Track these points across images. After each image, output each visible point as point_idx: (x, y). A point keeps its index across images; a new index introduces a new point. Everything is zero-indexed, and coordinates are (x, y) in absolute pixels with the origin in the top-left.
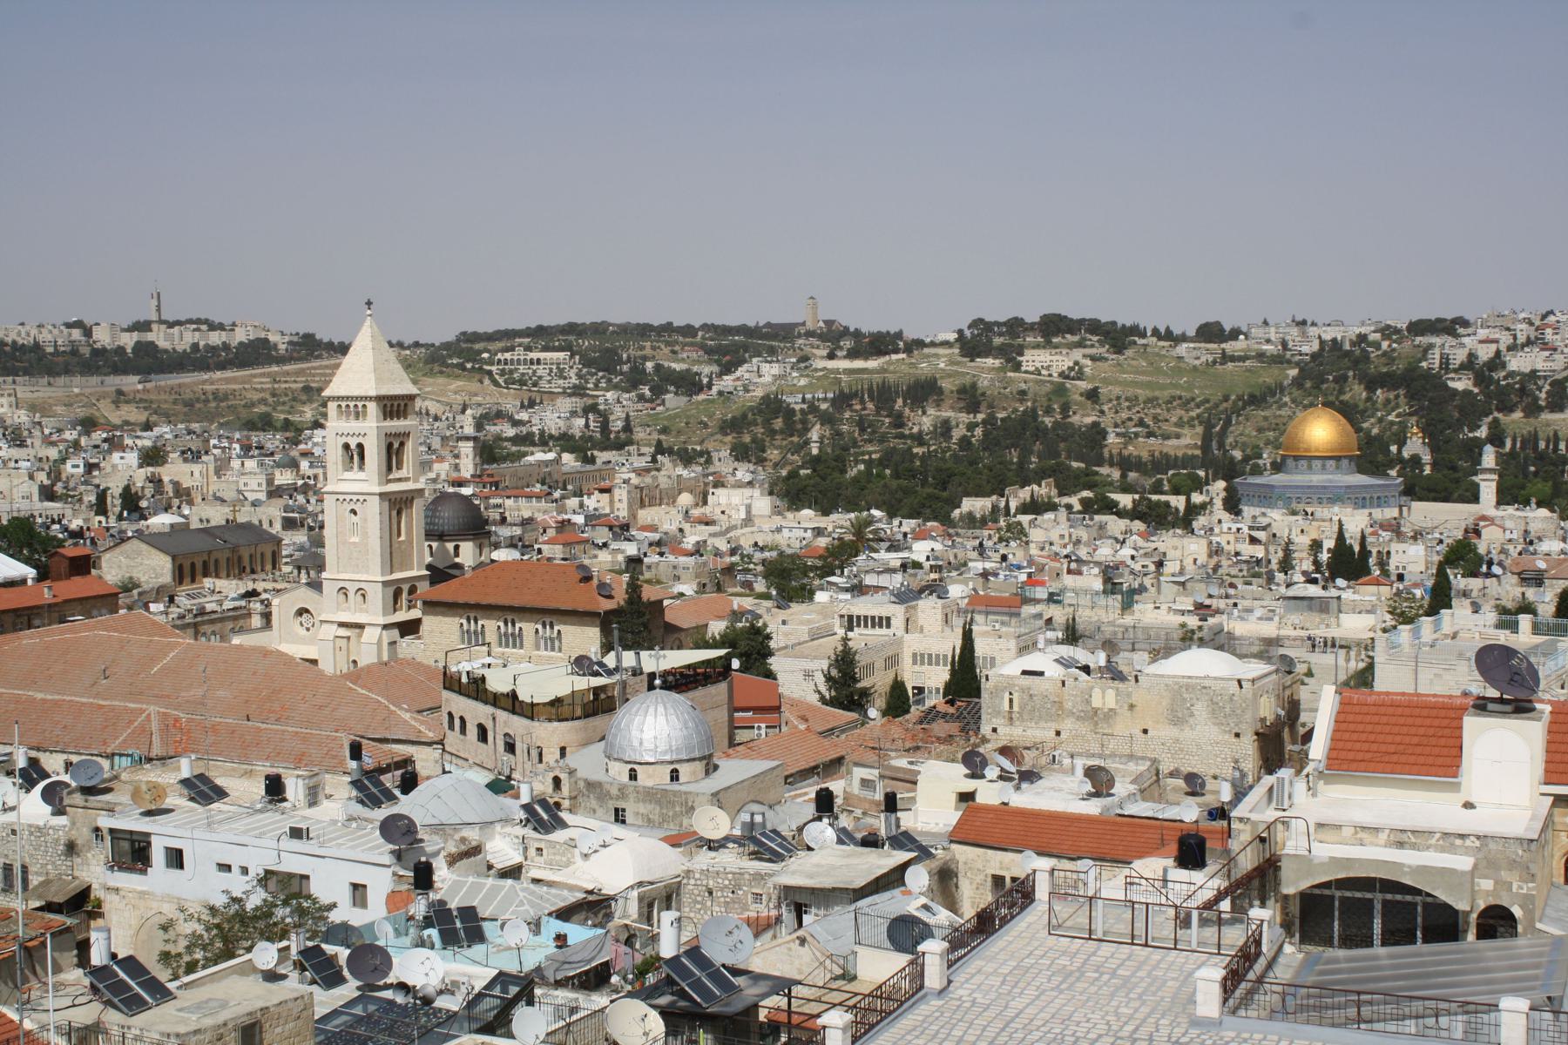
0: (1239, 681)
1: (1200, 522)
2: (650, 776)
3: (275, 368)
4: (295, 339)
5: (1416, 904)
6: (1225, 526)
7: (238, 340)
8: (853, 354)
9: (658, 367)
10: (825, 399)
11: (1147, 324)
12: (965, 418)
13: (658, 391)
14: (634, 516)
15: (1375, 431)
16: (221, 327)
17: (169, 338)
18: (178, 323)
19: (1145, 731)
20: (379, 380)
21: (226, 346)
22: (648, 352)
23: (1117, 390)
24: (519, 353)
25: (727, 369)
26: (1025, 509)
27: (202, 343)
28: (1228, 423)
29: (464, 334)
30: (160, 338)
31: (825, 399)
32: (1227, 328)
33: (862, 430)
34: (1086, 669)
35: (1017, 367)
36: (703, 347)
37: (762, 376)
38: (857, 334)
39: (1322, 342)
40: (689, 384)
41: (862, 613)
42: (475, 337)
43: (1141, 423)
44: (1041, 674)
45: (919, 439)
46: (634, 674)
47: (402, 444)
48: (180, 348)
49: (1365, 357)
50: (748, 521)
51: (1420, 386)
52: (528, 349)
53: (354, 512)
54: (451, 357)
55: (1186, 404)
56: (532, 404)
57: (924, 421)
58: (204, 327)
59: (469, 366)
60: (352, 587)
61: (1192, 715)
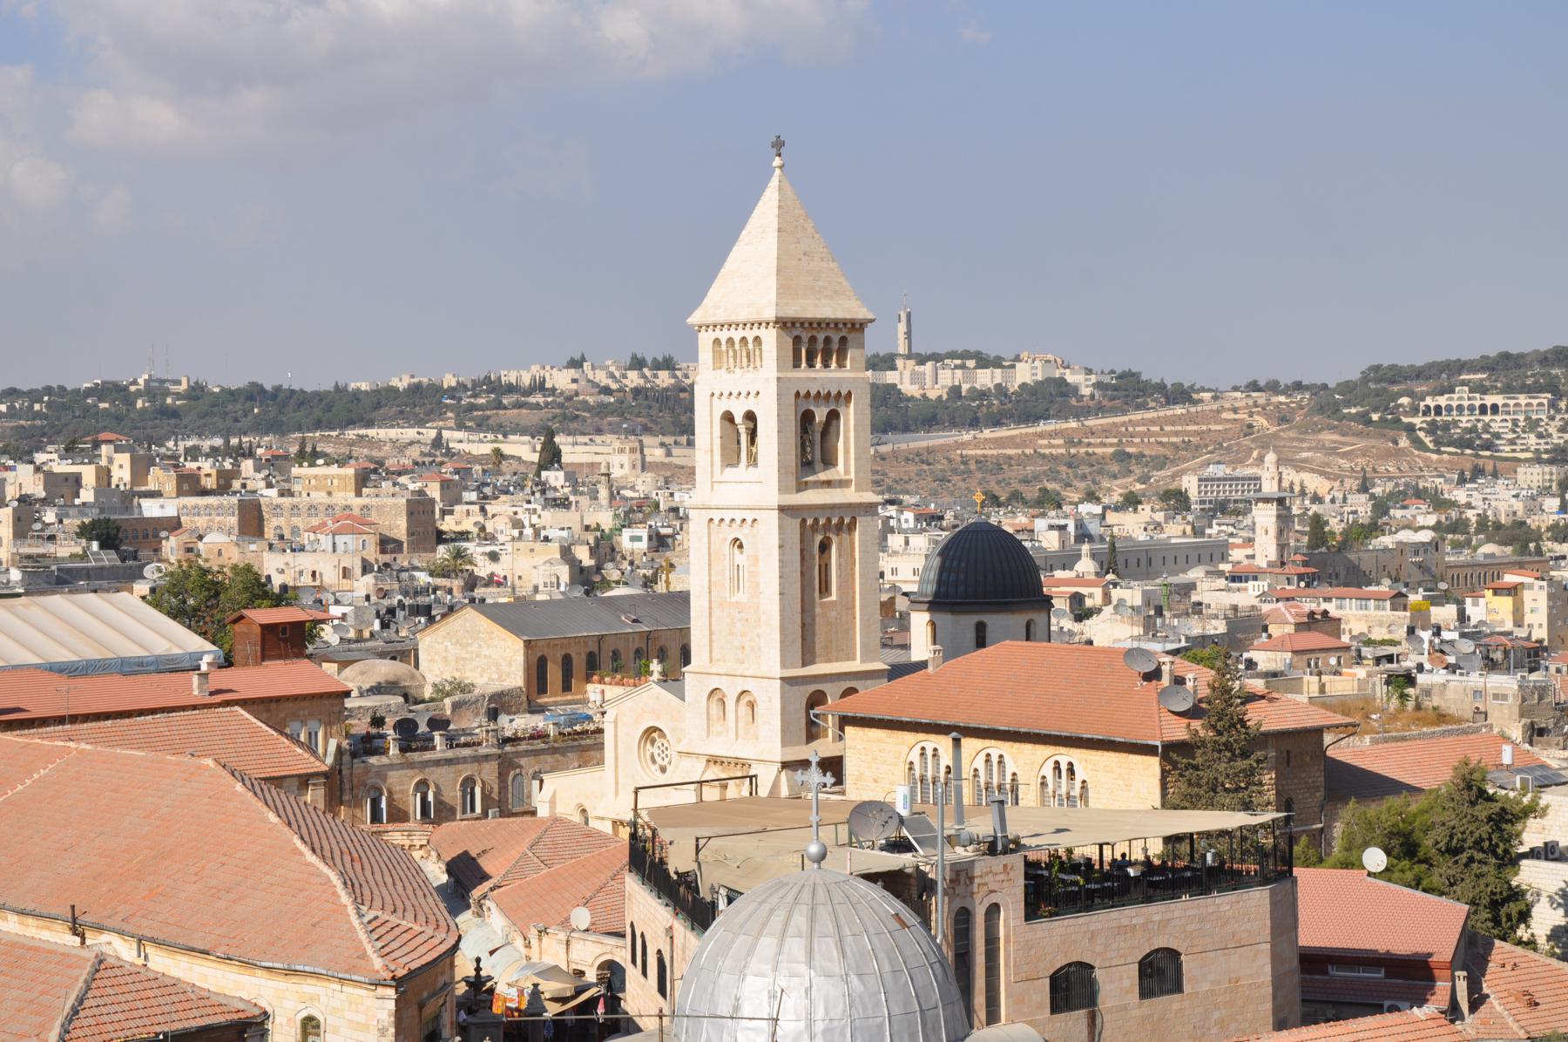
3: (1073, 424)
4: (1107, 379)
7: (1019, 381)
16: (997, 363)
17: (916, 378)
18: (936, 358)
21: (1001, 390)
24: (1461, 396)
27: (965, 387)
29: (1377, 368)
46: (992, 849)
47: (833, 416)
48: (933, 395)
52: (1482, 389)
53: (738, 544)
54: (1349, 404)
56: (1478, 472)
58: (971, 363)
59: (1375, 417)
60: (731, 690)
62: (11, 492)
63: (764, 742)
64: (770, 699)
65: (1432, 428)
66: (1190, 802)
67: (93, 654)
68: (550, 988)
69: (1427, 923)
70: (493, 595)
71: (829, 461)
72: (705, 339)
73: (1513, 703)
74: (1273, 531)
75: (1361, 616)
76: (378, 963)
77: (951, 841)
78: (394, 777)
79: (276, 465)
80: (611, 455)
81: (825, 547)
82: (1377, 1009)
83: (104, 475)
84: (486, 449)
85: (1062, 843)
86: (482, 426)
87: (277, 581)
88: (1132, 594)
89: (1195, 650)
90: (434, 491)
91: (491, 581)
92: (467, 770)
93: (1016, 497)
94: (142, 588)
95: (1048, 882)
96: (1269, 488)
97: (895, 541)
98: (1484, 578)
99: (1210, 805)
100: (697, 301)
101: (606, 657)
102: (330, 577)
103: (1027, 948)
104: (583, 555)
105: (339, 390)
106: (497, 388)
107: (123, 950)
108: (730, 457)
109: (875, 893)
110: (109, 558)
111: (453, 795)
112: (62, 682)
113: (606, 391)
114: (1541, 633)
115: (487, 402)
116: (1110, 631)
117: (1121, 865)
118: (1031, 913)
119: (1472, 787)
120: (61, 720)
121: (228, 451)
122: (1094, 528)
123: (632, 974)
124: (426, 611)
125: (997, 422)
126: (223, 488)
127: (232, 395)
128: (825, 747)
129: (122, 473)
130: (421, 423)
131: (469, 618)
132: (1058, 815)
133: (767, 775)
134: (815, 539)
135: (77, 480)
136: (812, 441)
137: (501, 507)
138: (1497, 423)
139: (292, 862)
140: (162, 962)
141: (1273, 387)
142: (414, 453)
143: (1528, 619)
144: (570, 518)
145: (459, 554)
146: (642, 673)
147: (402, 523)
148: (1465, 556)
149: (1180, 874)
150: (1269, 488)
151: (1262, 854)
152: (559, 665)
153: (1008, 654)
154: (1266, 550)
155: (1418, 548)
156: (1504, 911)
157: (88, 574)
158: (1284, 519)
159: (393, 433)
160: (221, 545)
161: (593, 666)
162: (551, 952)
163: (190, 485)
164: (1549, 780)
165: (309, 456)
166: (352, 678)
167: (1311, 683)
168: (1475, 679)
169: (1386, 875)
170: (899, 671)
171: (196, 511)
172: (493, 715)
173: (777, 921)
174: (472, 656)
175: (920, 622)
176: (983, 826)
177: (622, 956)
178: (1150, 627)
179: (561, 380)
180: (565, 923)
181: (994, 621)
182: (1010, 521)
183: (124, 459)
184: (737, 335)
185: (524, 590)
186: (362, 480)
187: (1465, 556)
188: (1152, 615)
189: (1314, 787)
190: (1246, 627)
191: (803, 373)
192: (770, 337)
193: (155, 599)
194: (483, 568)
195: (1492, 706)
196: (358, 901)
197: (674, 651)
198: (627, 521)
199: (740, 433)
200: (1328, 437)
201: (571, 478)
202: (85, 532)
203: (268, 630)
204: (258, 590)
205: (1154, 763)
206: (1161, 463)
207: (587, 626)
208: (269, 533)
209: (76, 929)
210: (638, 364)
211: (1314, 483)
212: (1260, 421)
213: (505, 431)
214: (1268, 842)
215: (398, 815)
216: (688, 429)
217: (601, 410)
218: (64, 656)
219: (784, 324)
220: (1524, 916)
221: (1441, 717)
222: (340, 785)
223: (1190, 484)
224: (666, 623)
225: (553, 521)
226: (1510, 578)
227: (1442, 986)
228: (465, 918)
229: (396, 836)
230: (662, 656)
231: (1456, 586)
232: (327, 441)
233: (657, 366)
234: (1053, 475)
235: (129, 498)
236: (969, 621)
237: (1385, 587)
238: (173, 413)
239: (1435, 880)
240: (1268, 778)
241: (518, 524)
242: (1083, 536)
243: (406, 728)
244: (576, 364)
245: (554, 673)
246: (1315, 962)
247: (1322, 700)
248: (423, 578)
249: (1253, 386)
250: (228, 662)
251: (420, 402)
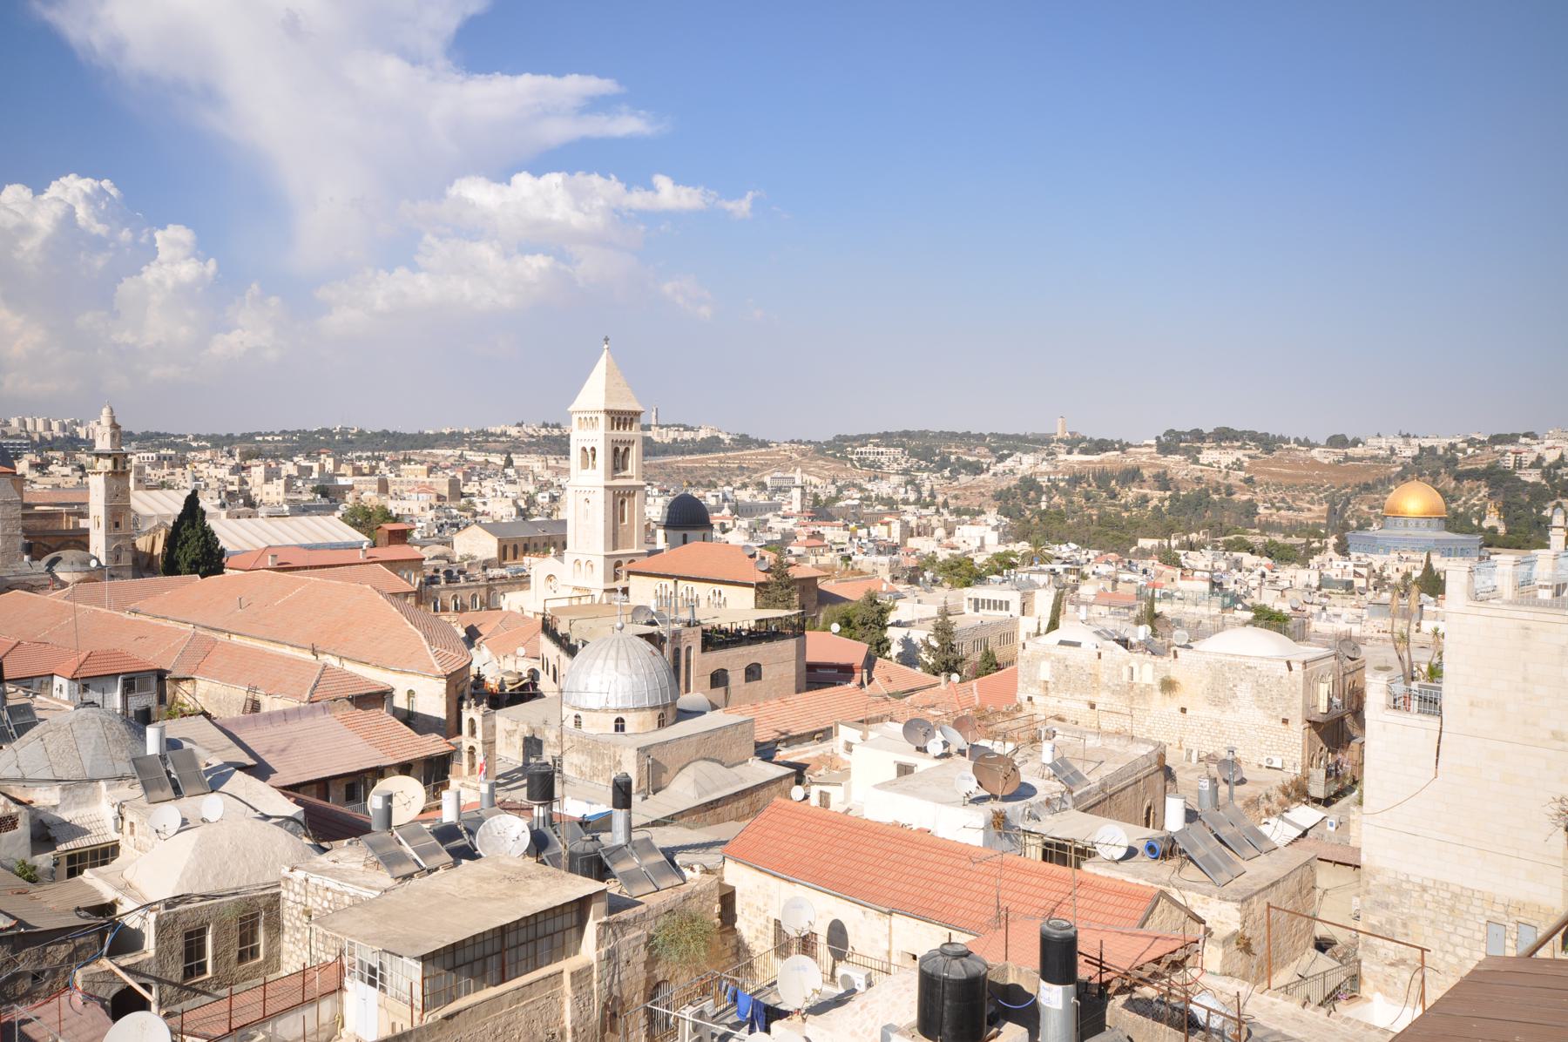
0: (1288, 663)
1: (1316, 560)
2: (593, 725)
6: (1334, 563)
8: (1084, 451)
9: (958, 459)
11: (1291, 434)
13: (955, 473)
14: (904, 543)
15: (1461, 510)
16: (692, 429)
17: (660, 435)
19: (1184, 710)
20: (608, 398)
23: (1266, 478)
25: (1001, 459)
26: (1181, 547)
28: (1348, 502)
32: (1350, 439)
33: (1088, 500)
34: (1125, 643)
35: (1196, 461)
36: (988, 446)
37: (1025, 464)
39: (1422, 449)
40: (976, 469)
41: (986, 597)
42: (846, 439)
43: (1283, 500)
44: (1078, 645)
45: (1126, 507)
46: (689, 625)
47: (627, 449)
49: (1455, 461)
50: (981, 548)
51: (1497, 478)
52: (877, 446)
55: (1317, 489)
56: (876, 477)
57: (1131, 494)
60: (583, 560)
61: (1234, 696)
62: (284, 473)
63: (596, 581)
64: (599, 564)
65: (859, 460)
66: (766, 606)
67: (319, 541)
68: (507, 678)
69: (852, 651)
70: (484, 520)
71: (625, 468)
72: (575, 418)
73: (887, 567)
75: (832, 533)
76: (439, 669)
77: (673, 621)
78: (443, 593)
79: (394, 464)
80: (534, 462)
81: (623, 503)
82: (834, 685)
83: (322, 467)
84: (482, 459)
85: (716, 623)
86: (480, 449)
87: (394, 513)
88: (744, 523)
89: (768, 546)
90: (460, 476)
91: (483, 513)
92: (474, 591)
93: (699, 484)
94: (338, 514)
95: (712, 638)
96: (798, 482)
97: (650, 500)
98: (876, 518)
99: (774, 607)
100: (572, 402)
101: (531, 547)
102: (416, 511)
103: (702, 663)
104: (522, 504)
105: (421, 434)
106: (486, 434)
107: (333, 662)
108: (585, 465)
109: (643, 642)
110: (325, 502)
111: (468, 601)
112: (307, 553)
114: (897, 540)
115: (482, 440)
116: (736, 538)
117: (739, 631)
118: (704, 650)
119: (872, 600)
120: (306, 568)
121: (374, 458)
122: (730, 496)
123: (542, 674)
124: (457, 525)
126: (372, 473)
127: (375, 434)
128: (619, 585)
129: (329, 465)
130: (454, 448)
131: (475, 529)
132: (714, 611)
133: (598, 594)
134: (619, 499)
135: (311, 469)
136: (618, 459)
137: (488, 483)
138: (883, 459)
139: (401, 626)
140: (349, 667)
141: (800, 442)
142: (451, 460)
144: (517, 488)
145: (470, 502)
146: (547, 552)
148: (871, 510)
149: (761, 634)
150: (798, 482)
151: (793, 626)
152: (514, 547)
153: (695, 548)
154: (796, 507)
155: (853, 507)
156: (881, 646)
157: (316, 508)
158: (804, 494)
160: (370, 496)
161: (526, 549)
162: (509, 665)
163: (358, 472)
164: (899, 596)
165: (408, 460)
166: (427, 553)
167: (813, 559)
168: (874, 558)
169: (840, 633)
170: (652, 553)
171: (360, 482)
172: (485, 569)
173: (603, 653)
174: (476, 544)
175: (660, 533)
176: (685, 615)
177: (538, 667)
178: (751, 537)
179: (513, 431)
180: (514, 653)
181: (689, 533)
182: (696, 493)
183: (331, 460)
185: (497, 518)
186: (430, 471)
187: (871, 510)
188: (752, 531)
189: (813, 596)
190: (788, 537)
191: (615, 432)
192: (602, 417)
193: (344, 518)
194: (480, 508)
195: (879, 568)
196: (431, 644)
197: (560, 544)
198: (541, 490)
199: (589, 455)
200: (820, 462)
201: (517, 472)
202: (314, 490)
203: (391, 532)
204: (387, 516)
205: (752, 591)
206: (756, 471)
207: (524, 533)
208: (391, 492)
209: (314, 652)
210: (545, 425)
211: (815, 480)
212: (794, 455)
213: (489, 451)
214: (796, 621)
215: (445, 609)
216: (567, 453)
217: (530, 444)
218: (307, 542)
219: (608, 412)
220: (888, 648)
221: (861, 573)
222: (421, 597)
223: (767, 480)
224: (555, 532)
225: (509, 489)
226: (887, 519)
227: (857, 676)
228: (473, 650)
229: (444, 617)
230: (555, 545)
231: (866, 521)
232: (415, 455)
233: (553, 427)
234: (714, 475)
235: (332, 476)
236: (680, 534)
237: (841, 522)
238: (351, 442)
239: (857, 635)
240: (796, 596)
241: (495, 490)
242: (725, 499)
243: (448, 573)
244: (519, 425)
245: (510, 552)
246: (812, 667)
247: (817, 566)
248: (455, 512)
249: (792, 442)
250: (374, 545)
251: (455, 439)
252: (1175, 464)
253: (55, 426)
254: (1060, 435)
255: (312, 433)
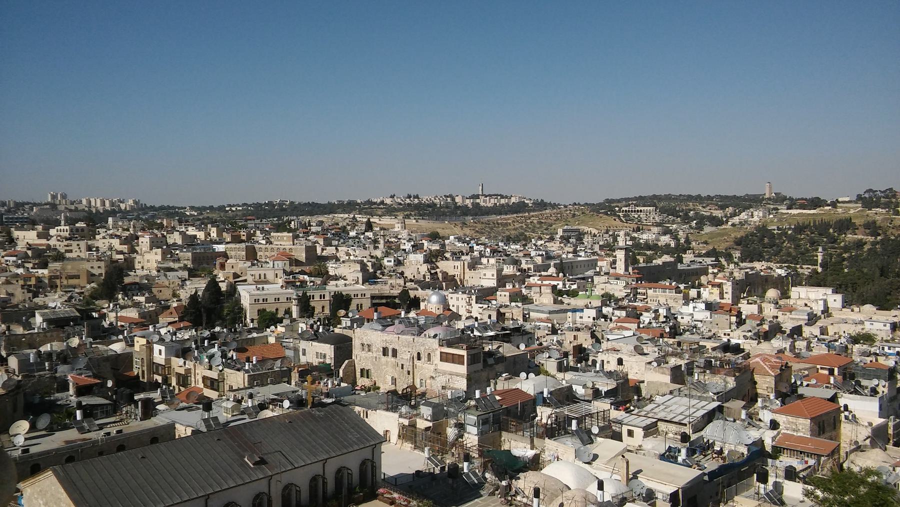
5: (29, 354)
10: (790, 229)
12: (871, 239)
16: (506, 197)
17: (485, 201)
18: (490, 196)
22: (691, 207)
30: (481, 201)
31: (790, 229)
38: (791, 199)
40: (716, 222)
42: (612, 201)
52: (636, 205)
74: (623, 260)
86: (366, 213)
113: (400, 204)
125: (506, 214)
142: (347, 221)
143: (725, 296)
147: (304, 255)
159: (342, 215)
179: (388, 201)
183: (214, 229)
184: (356, 447)
198: (387, 254)
210: (409, 197)
238: (285, 210)
252: (878, 214)
253: (107, 203)
254: (767, 196)
255: (261, 205)
